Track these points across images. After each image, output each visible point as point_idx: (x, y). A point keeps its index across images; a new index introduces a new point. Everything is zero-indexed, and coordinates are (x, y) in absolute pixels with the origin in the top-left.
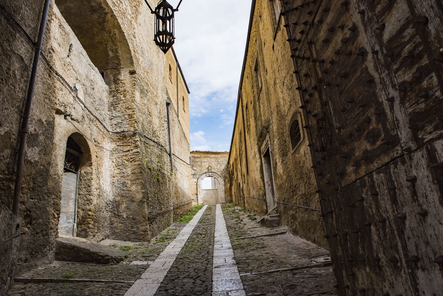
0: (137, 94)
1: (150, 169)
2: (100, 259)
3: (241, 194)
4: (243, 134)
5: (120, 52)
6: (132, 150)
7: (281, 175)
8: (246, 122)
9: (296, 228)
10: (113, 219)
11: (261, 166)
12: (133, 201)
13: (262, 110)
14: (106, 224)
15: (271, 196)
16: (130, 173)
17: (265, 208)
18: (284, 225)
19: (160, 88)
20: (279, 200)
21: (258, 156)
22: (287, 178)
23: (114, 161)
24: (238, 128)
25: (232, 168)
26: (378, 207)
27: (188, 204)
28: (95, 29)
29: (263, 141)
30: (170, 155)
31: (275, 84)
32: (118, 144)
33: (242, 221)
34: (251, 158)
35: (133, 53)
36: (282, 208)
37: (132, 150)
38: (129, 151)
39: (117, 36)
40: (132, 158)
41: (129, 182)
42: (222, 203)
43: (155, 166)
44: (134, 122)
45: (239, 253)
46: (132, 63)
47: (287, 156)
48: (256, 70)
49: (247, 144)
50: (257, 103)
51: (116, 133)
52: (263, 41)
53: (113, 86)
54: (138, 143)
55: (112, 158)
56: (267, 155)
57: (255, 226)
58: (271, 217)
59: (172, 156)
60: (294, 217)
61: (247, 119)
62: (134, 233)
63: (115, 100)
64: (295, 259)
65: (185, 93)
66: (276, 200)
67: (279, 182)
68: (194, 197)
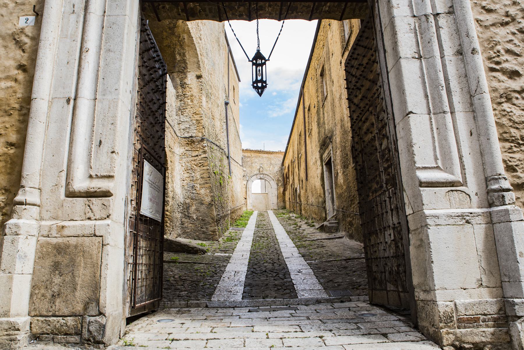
0: (204, 99)
1: (215, 173)
2: (190, 250)
3: (298, 201)
4: (303, 137)
5: (187, 56)
6: (200, 155)
7: (341, 185)
8: (307, 125)
9: (352, 233)
10: (183, 220)
11: (322, 174)
12: (202, 204)
13: (326, 118)
14: (178, 224)
15: (331, 204)
16: (199, 177)
17: (324, 215)
19: (221, 89)
20: (338, 208)
21: (319, 163)
22: (347, 188)
23: (184, 165)
24: (298, 128)
25: (287, 170)
26: (378, 210)
27: (240, 209)
28: (165, 33)
29: (325, 149)
30: (228, 157)
31: (340, 98)
32: (186, 148)
33: (300, 227)
34: (311, 164)
35: (200, 57)
36: (341, 215)
37: (200, 155)
38: (197, 156)
39: (186, 40)
40: (200, 163)
41: (198, 186)
42: (274, 210)
43: (217, 170)
44: (201, 127)
45: (302, 250)
46: (199, 67)
47: (347, 168)
48: (322, 75)
49: (307, 148)
50: (321, 110)
51: (184, 138)
52: (331, 51)
53: (180, 90)
54: (206, 148)
55: (181, 162)
56: (329, 164)
57: (314, 231)
58: (330, 223)
59: (231, 160)
60: (351, 224)
61: (309, 122)
62: (204, 233)
63: (183, 105)
64: (348, 254)
65: (235, 81)
66: (336, 208)
67: (339, 191)
68: (243, 201)
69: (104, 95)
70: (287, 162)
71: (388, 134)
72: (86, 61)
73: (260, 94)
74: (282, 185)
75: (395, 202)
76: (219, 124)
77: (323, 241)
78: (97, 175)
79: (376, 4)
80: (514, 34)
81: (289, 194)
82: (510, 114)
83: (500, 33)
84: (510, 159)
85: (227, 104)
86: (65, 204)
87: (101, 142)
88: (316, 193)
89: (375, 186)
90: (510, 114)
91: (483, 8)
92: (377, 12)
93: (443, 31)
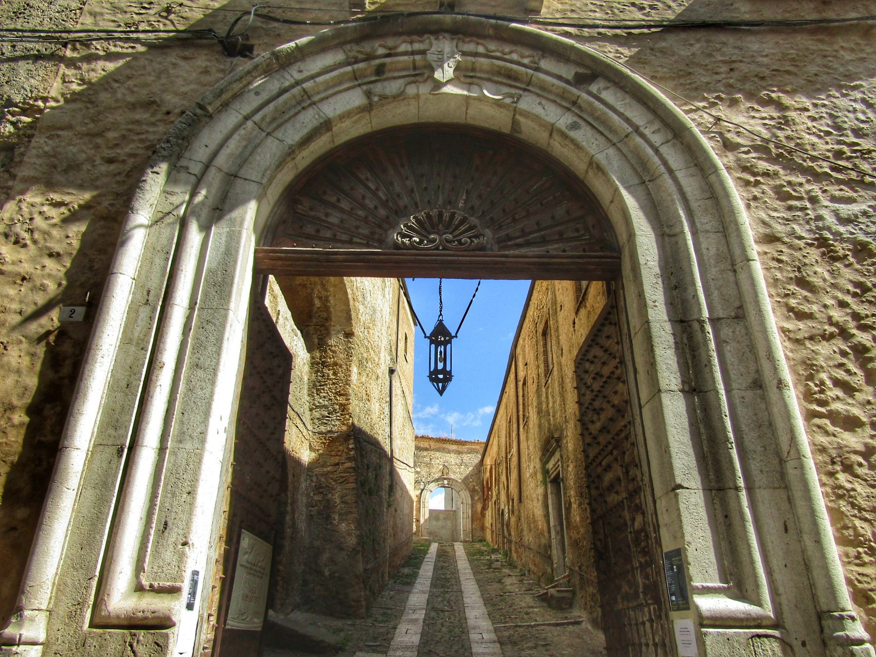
4: (515, 426)
8: (521, 407)
11: (545, 496)
12: (341, 549)
13: (551, 405)
16: (338, 501)
18: (580, 607)
19: (383, 349)
25: (488, 474)
38: (338, 464)
40: (342, 477)
49: (521, 447)
58: (558, 591)
69: (181, 442)
70: (488, 462)
71: (644, 506)
72: (159, 383)
73: (441, 392)
74: (479, 499)
75: (660, 633)
76: (376, 407)
77: (548, 628)
78: (151, 586)
79: (621, 291)
80: (844, 354)
81: (492, 517)
82: (852, 493)
83: (823, 352)
84: (859, 578)
85: (392, 371)
86: (89, 641)
87: (166, 524)
88: (536, 527)
89: (625, 588)
90: (852, 493)
91: (791, 309)
92: (622, 303)
93: (728, 348)
